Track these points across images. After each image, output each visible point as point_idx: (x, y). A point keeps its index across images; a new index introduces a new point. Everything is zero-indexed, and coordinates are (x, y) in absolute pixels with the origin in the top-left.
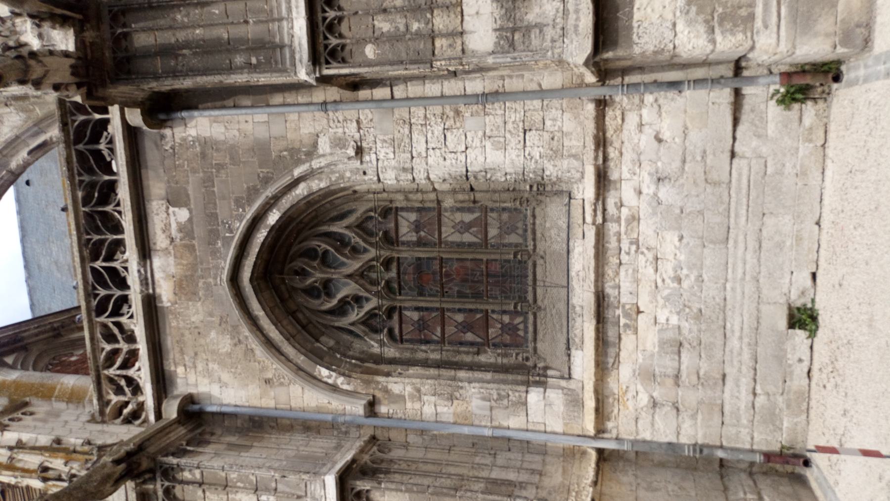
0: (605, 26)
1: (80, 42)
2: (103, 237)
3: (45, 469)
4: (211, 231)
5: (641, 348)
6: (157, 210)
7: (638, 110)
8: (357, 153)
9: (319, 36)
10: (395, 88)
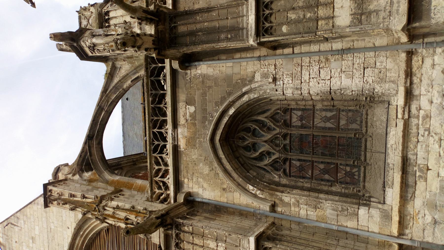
0: (415, 10)
1: (156, 30)
2: (158, 118)
3: (127, 219)
4: (203, 117)
5: (428, 189)
6: (181, 107)
7: (432, 57)
8: (273, 81)
9: (260, 22)
10: (294, 48)
